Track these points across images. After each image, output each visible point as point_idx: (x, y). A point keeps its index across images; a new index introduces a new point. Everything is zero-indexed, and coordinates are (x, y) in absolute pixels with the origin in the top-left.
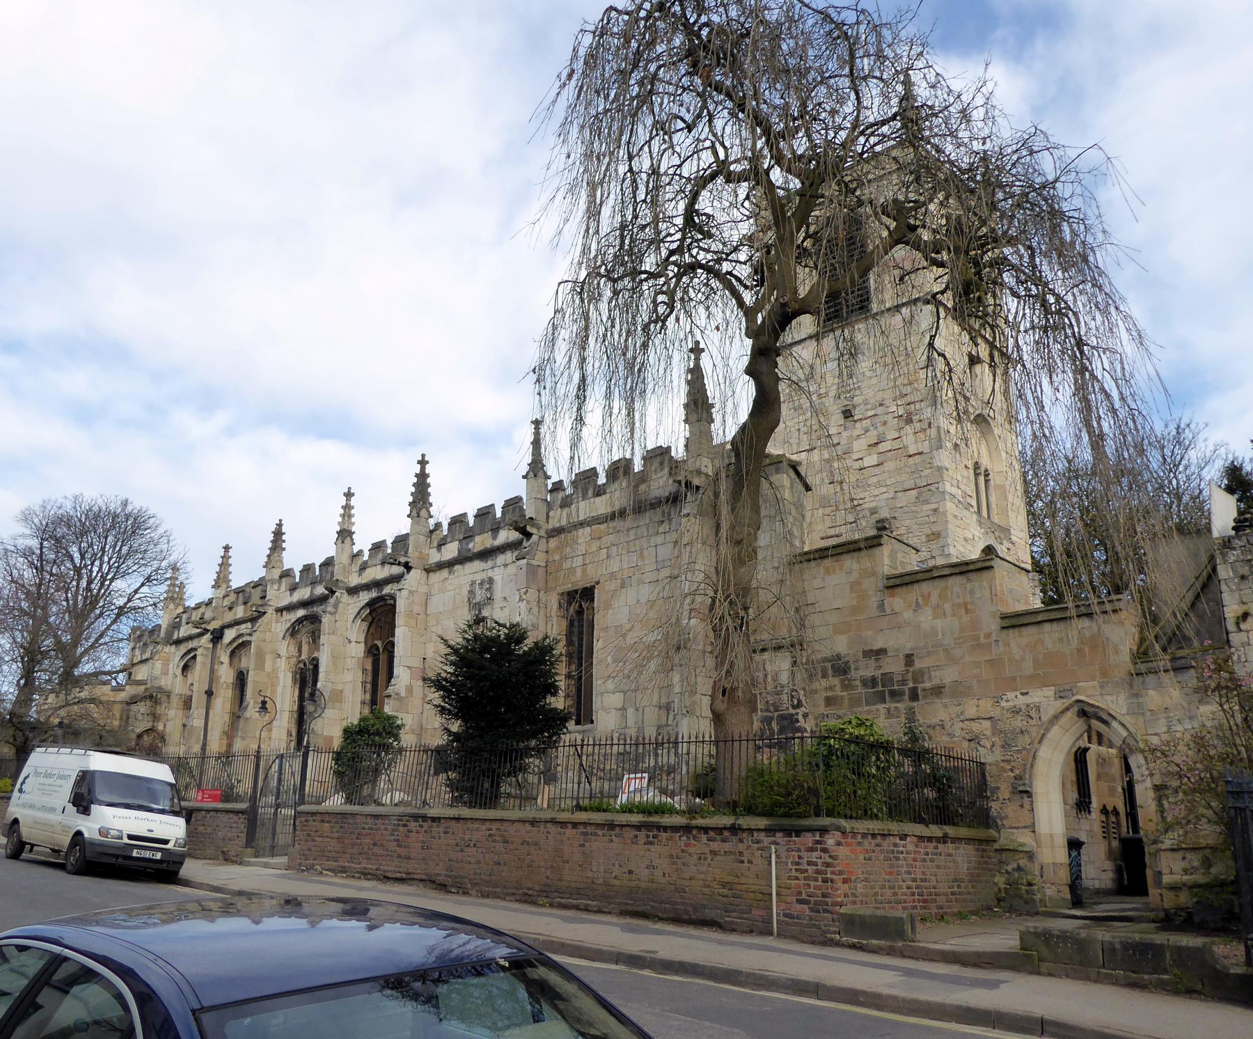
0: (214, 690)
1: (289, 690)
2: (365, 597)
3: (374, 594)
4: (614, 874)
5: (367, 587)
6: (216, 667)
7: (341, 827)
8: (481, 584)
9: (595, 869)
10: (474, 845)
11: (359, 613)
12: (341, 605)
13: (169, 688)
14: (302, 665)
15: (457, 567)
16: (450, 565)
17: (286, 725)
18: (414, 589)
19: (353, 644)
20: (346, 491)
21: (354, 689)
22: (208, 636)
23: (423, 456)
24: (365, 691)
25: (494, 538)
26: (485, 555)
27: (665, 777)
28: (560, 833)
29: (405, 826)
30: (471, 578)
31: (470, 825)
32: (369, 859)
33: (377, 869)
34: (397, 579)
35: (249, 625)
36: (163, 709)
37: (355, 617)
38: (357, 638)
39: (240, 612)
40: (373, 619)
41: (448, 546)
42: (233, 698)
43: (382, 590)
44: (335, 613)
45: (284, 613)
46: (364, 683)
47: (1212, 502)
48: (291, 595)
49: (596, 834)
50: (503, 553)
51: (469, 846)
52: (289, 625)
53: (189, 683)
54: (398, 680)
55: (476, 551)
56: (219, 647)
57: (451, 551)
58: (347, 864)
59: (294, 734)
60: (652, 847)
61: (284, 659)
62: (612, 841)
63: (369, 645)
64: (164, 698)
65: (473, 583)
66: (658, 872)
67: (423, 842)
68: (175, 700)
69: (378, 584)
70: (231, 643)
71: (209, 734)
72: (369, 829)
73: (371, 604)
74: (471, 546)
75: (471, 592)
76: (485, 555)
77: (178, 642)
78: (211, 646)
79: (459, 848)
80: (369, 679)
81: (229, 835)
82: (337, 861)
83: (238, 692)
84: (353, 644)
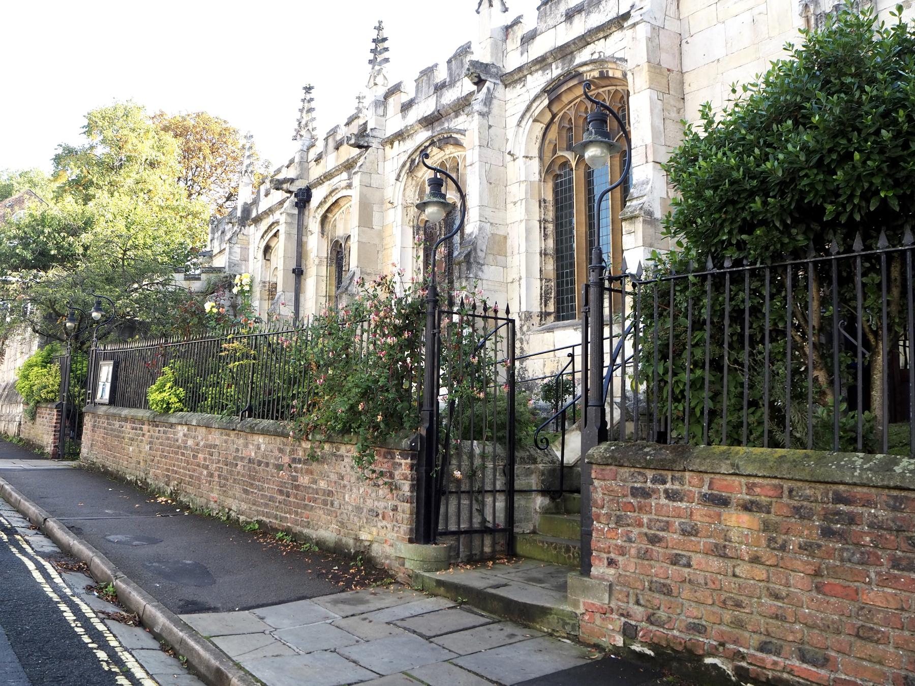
0: (303, 268)
1: (410, 253)
2: (537, 81)
3: (556, 71)
5: (542, 63)
6: (304, 239)
7: (827, 533)
11: (528, 109)
12: (495, 102)
18: (659, 23)
19: (521, 161)
20: (377, 25)
21: (528, 231)
23: (380, 22)
24: (546, 235)
35: (345, 175)
37: (522, 117)
38: (527, 150)
40: (554, 116)
42: (328, 277)
43: (572, 61)
44: (488, 113)
45: (396, 143)
46: (543, 222)
48: (404, 117)
52: (404, 157)
53: (273, 268)
56: (306, 213)
61: (400, 208)
63: (548, 162)
69: (564, 52)
73: (552, 91)
78: (296, 211)
80: (551, 215)
81: (369, 503)
83: (334, 268)
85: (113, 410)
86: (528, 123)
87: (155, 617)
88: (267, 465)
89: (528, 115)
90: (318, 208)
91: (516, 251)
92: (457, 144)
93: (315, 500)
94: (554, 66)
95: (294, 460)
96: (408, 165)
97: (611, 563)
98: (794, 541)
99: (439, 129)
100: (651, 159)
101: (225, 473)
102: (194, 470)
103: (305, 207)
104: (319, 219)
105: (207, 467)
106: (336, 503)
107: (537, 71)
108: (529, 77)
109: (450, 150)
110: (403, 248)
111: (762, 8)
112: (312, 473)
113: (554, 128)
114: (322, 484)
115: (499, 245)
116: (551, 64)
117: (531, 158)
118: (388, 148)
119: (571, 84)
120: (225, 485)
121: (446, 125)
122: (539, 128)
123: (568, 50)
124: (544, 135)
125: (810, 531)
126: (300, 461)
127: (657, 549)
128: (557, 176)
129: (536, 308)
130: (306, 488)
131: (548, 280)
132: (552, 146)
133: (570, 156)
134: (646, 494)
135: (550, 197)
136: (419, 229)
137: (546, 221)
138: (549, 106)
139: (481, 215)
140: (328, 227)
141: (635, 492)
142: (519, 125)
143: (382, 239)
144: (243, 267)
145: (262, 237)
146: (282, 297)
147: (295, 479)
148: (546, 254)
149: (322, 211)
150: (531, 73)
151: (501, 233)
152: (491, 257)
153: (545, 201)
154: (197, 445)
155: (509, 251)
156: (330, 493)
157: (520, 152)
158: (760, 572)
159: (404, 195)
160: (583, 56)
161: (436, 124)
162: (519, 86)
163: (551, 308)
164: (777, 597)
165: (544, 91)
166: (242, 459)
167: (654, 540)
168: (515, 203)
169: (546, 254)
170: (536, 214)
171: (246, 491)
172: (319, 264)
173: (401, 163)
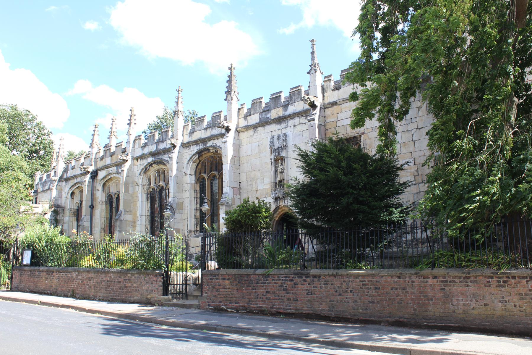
0: (94, 205)
1: (145, 204)
2: (195, 149)
3: (201, 147)
4: (472, 307)
5: (196, 142)
6: (95, 192)
7: (239, 282)
8: (278, 137)
9: (455, 304)
10: (351, 291)
11: (191, 158)
13: (63, 205)
14: (151, 190)
15: (260, 129)
16: (255, 127)
17: (144, 223)
19: (188, 176)
21: (191, 201)
22: (89, 176)
24: (197, 203)
25: (285, 110)
26: (280, 120)
27: (420, 245)
28: (423, 282)
29: (292, 280)
30: (270, 135)
31: (345, 279)
32: (264, 301)
33: (271, 308)
34: (222, 136)
35: (115, 168)
36: (61, 217)
37: (189, 160)
39: (108, 161)
40: (200, 161)
41: (252, 116)
42: (106, 210)
43: (206, 144)
45: (139, 160)
47: (58, 167)
48: (143, 150)
49: (454, 282)
50: (292, 119)
51: (347, 291)
52: (143, 167)
54: (227, 195)
55: (272, 118)
56: (95, 181)
57: (255, 119)
58: (246, 305)
59: (149, 228)
60: (503, 289)
61: (140, 186)
62: (468, 286)
64: (61, 211)
65: (273, 137)
66: (510, 306)
67: (307, 290)
68: (67, 212)
69: (204, 141)
70: (103, 178)
71: (93, 229)
72: (262, 283)
73: (200, 153)
74: (268, 116)
75: (272, 143)
76: (280, 120)
77: (67, 180)
78: (91, 181)
79: (338, 293)
80: (199, 196)
81: (150, 288)
82: (238, 303)
83: (108, 205)
84: (188, 176)
85: (32, 268)
86: (191, 163)
87: (280, 216)
88: (114, 282)
89: (191, 160)
90: (102, 180)
91: (186, 208)
92: (164, 164)
93: (133, 290)
94: (200, 145)
95: (125, 280)
96: (144, 169)
97: (206, 293)
98: (235, 284)
99: (157, 158)
100: (228, 186)
101: (96, 286)
102: (82, 286)
103: (95, 178)
104: (102, 185)
105: (88, 285)
106: (140, 290)
107: (194, 145)
108: (192, 146)
109: (161, 166)
110: (142, 202)
111: (261, 142)
112: (131, 282)
113: (200, 165)
114: (135, 285)
115: (181, 205)
116: (199, 144)
117: (192, 175)
118: (135, 161)
119: (206, 152)
120: (97, 290)
121: (160, 157)
122: (195, 165)
123: (206, 140)
124: (197, 167)
125: (236, 282)
126: (127, 280)
127: (214, 289)
128: (201, 182)
129: (193, 229)
130: (130, 287)
131: (197, 219)
132: (199, 171)
133: (205, 175)
134: (212, 279)
135: (198, 189)
136: (148, 194)
137: (197, 198)
138: (198, 158)
139: (174, 196)
140: (106, 188)
141: (211, 279)
142: (188, 163)
143: (133, 198)
144: (59, 201)
145: (70, 188)
146: (85, 218)
147: (125, 285)
148: (197, 210)
149: (103, 182)
150: (192, 145)
151: (181, 201)
152: (177, 210)
153: (196, 190)
154: (83, 278)
155: (184, 208)
156: (138, 287)
157: (188, 173)
158: (230, 290)
159: (142, 181)
160: (210, 144)
161: (156, 156)
162: (188, 149)
163: (198, 228)
164: (232, 294)
165: (197, 153)
166: (104, 281)
167: (214, 287)
168: (186, 191)
169: (197, 210)
170: (193, 195)
171: (106, 290)
172: (102, 204)
173: (142, 168)
